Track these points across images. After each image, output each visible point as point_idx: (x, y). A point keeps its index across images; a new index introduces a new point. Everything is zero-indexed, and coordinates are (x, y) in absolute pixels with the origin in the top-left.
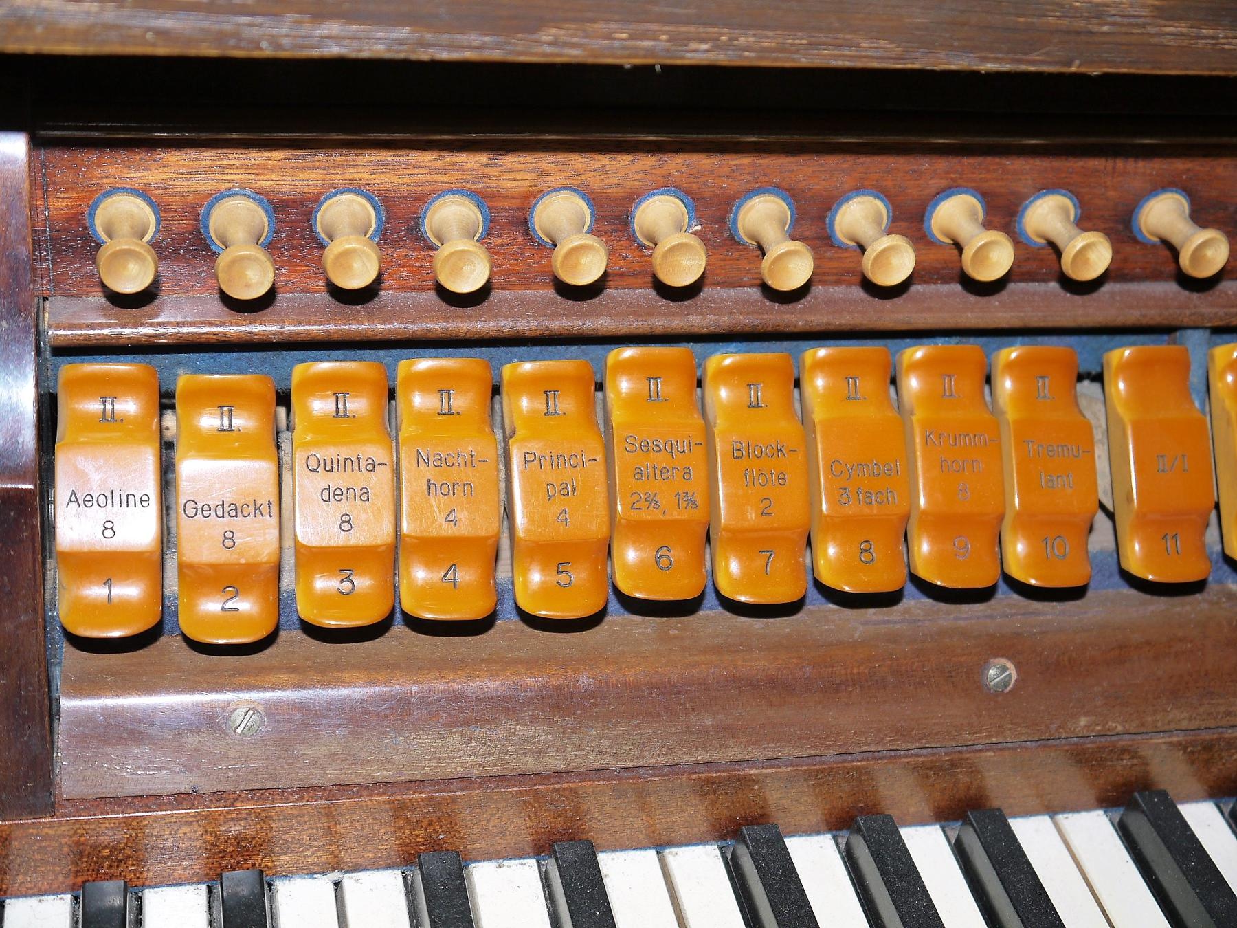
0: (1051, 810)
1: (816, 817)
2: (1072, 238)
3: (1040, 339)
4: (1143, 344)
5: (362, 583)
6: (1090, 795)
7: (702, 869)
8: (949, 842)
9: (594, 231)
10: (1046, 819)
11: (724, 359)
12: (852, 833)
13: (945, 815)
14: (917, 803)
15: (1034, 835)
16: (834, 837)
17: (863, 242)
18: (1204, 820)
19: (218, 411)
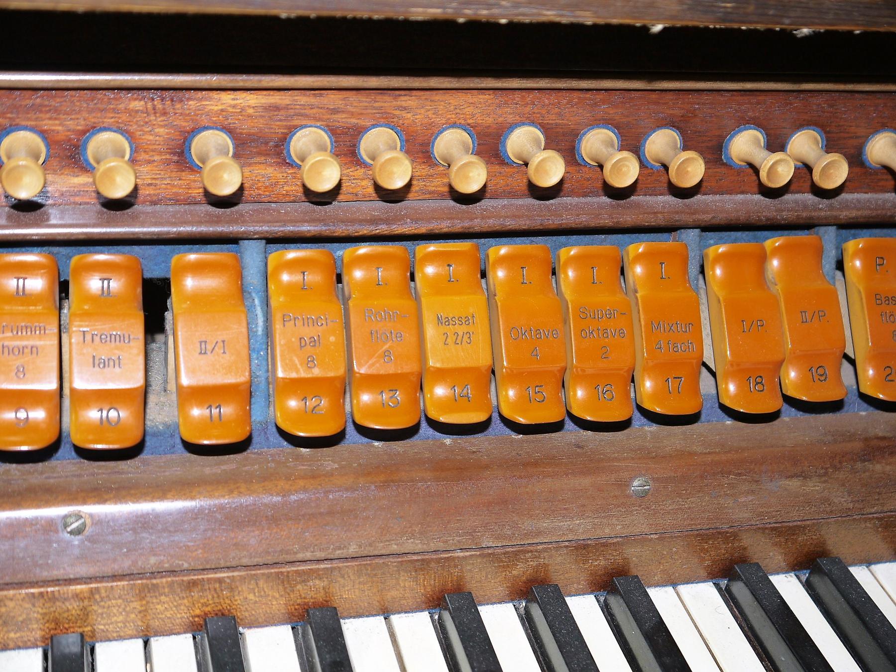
0: (868, 562)
1: (502, 590)
2: (819, 158)
3: (518, 240)
4: (735, 241)
5: (228, 410)
6: (703, 573)
7: (418, 630)
8: (801, 581)
10: (670, 589)
11: (500, 250)
13: (795, 567)
19: (27, 292)
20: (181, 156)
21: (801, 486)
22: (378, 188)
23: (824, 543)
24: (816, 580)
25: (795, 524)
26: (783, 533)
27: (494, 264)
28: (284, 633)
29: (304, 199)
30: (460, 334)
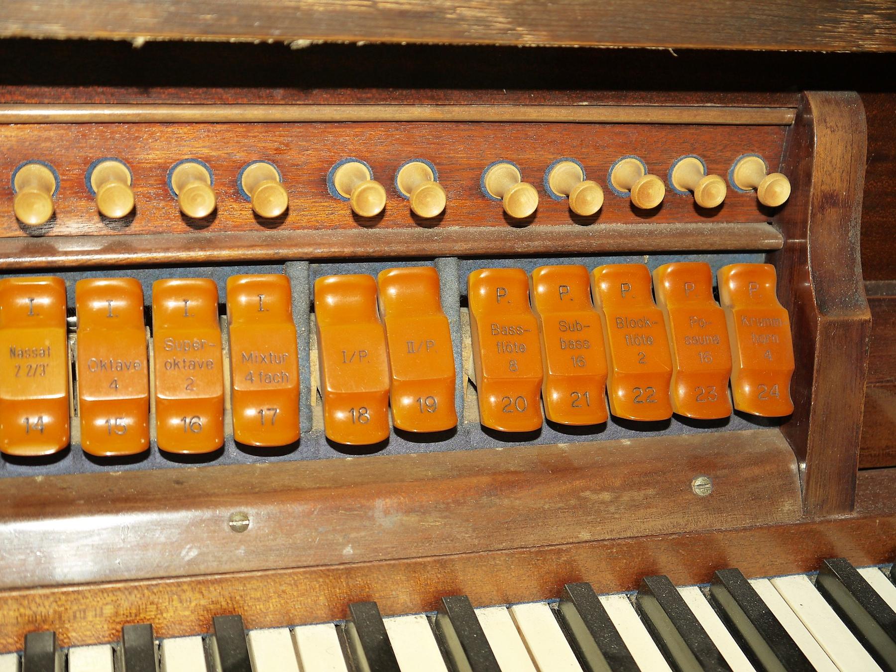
0: (769, 575)
9: (708, 172)
12: (713, 584)
13: (878, 561)
14: (608, 578)
15: (493, 622)
16: (700, 589)
17: (692, 188)
18: (875, 578)
20: (322, 185)
21: (419, 521)
22: (257, 216)
23: (654, 563)
24: (828, 583)
25: (359, 565)
26: (682, 542)
27: (599, 279)
28: (195, 644)
29: (355, 224)
30: (34, 366)
